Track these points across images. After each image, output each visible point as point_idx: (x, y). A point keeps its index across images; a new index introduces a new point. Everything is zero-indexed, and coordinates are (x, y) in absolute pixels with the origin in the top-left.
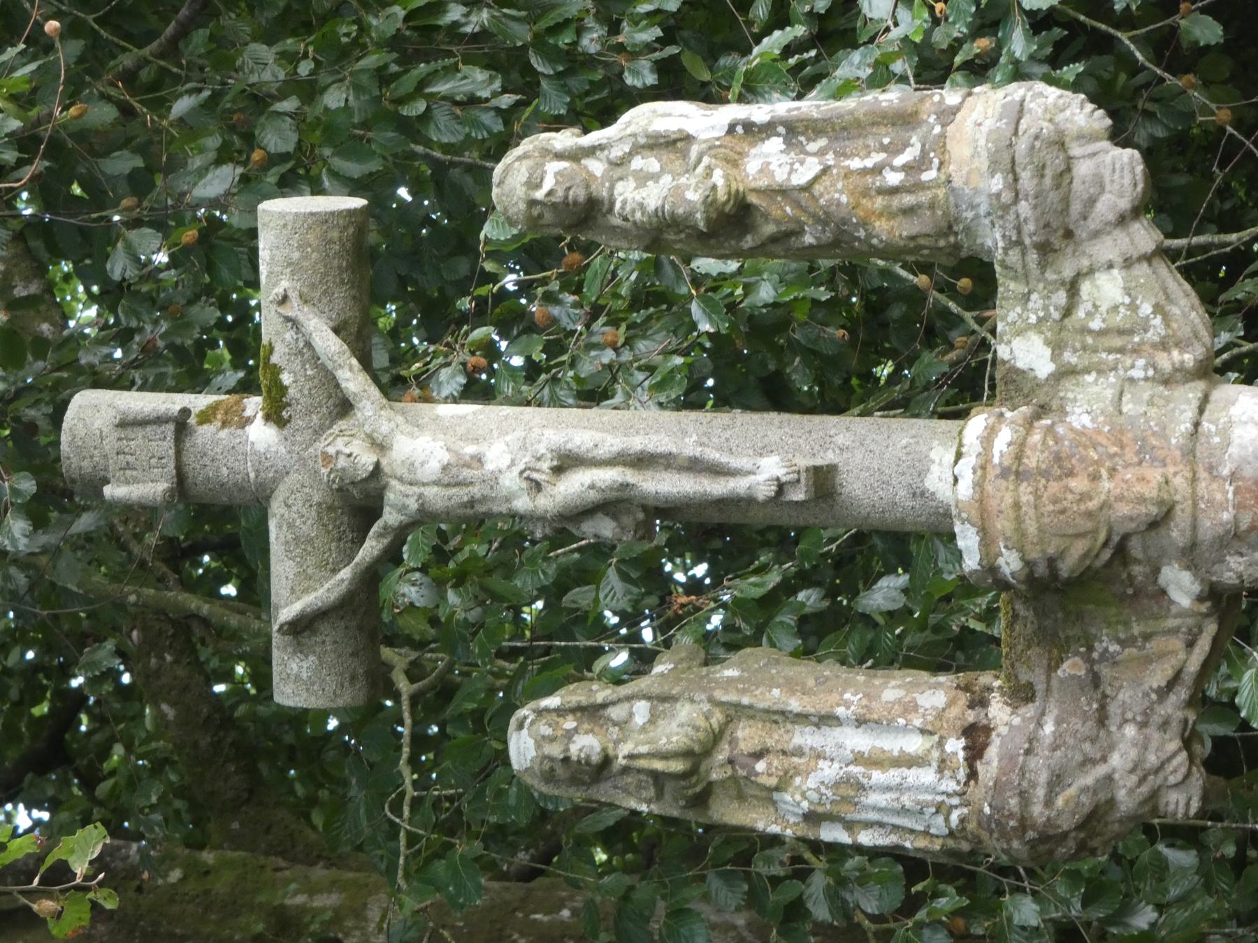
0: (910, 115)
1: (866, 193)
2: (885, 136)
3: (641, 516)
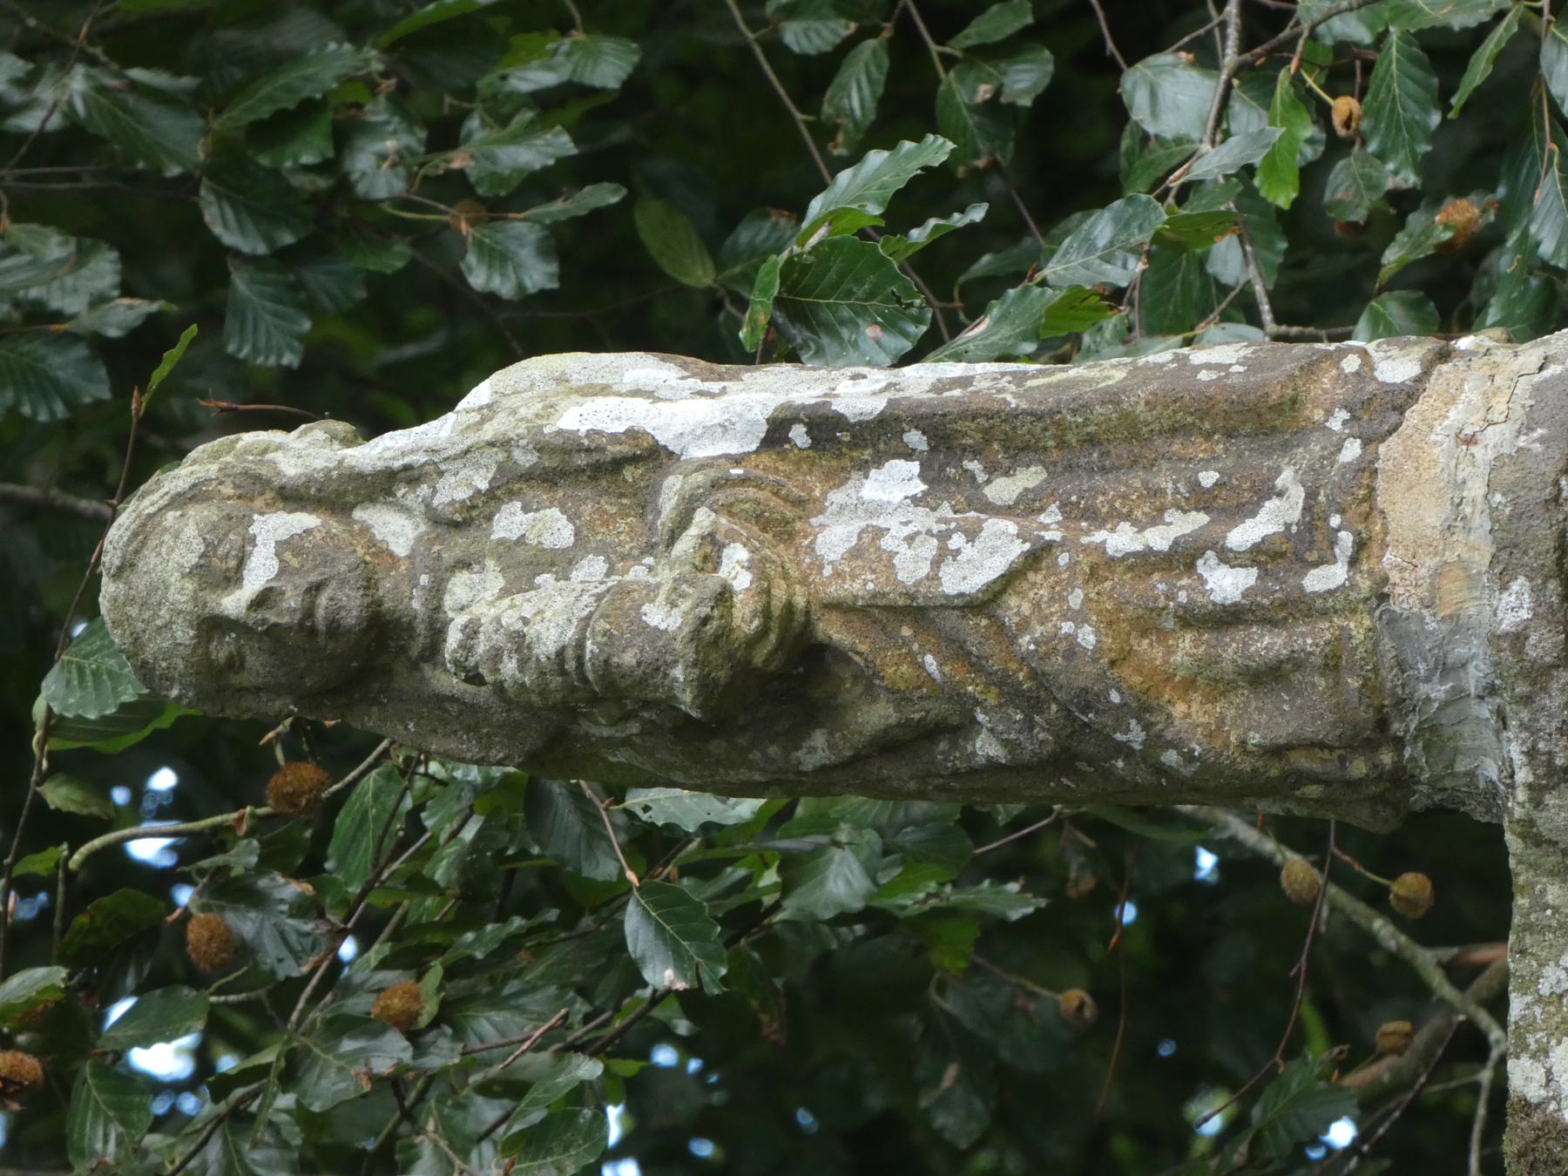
0: (1278, 408)
1: (1148, 623)
2: (1206, 464)
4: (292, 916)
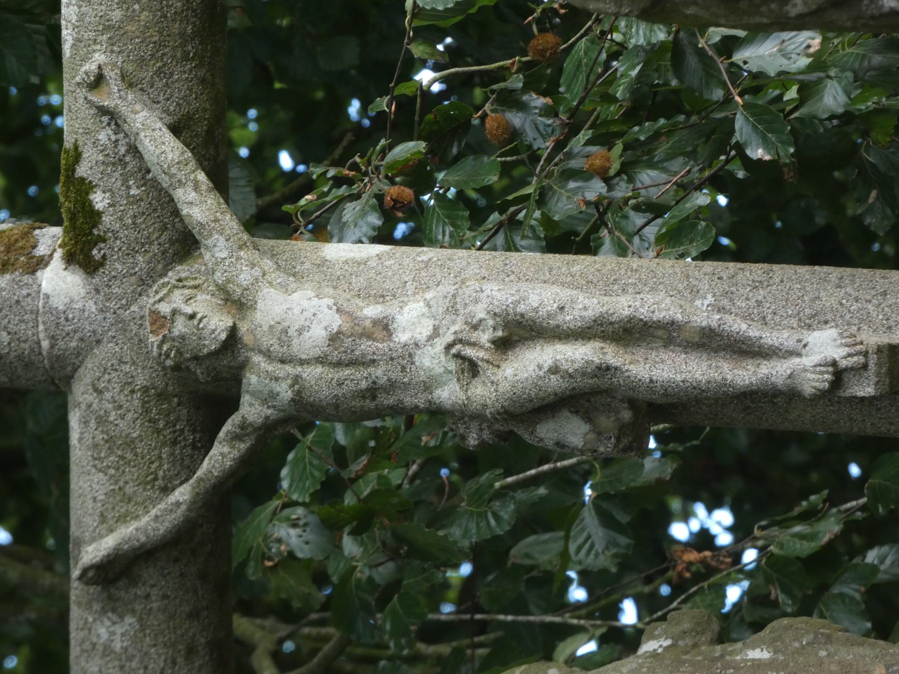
3: (627, 415)
4: (541, 116)
